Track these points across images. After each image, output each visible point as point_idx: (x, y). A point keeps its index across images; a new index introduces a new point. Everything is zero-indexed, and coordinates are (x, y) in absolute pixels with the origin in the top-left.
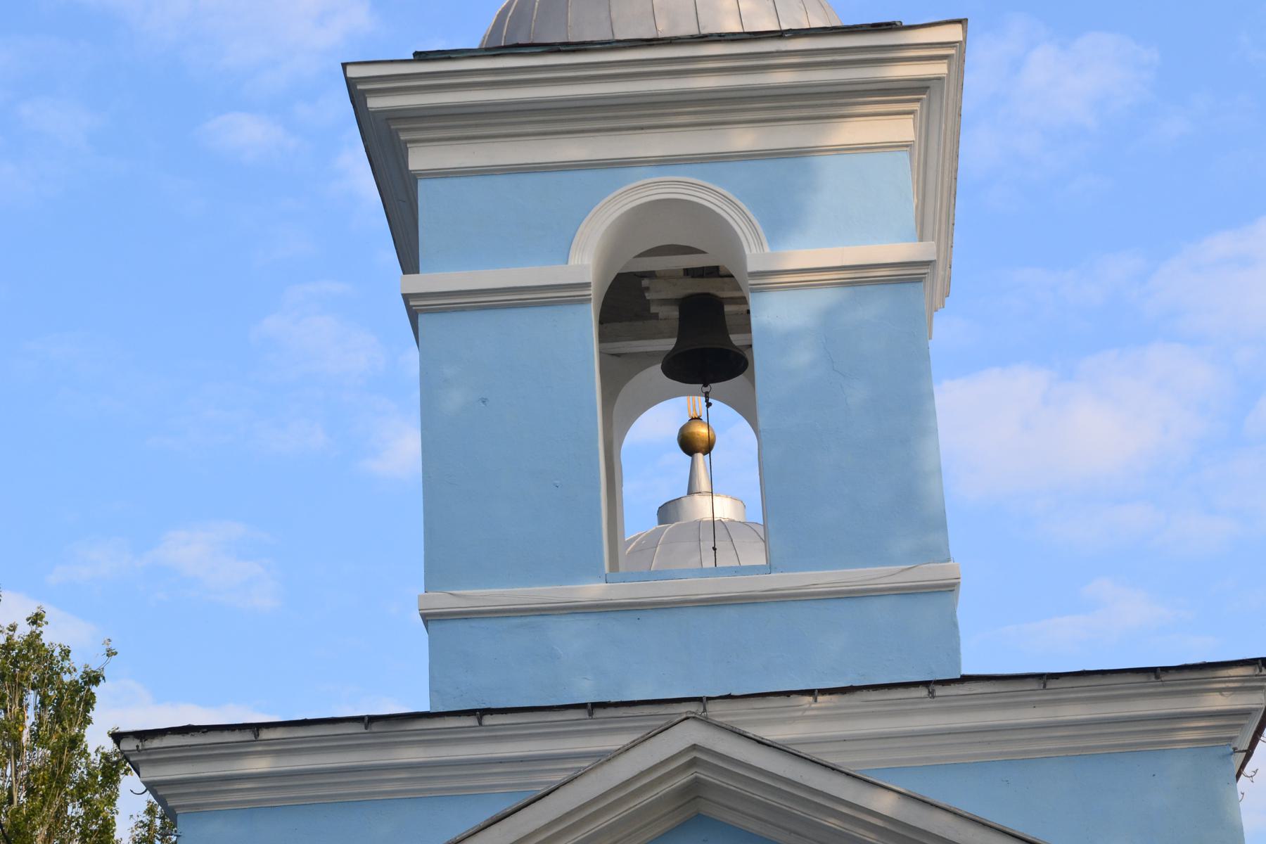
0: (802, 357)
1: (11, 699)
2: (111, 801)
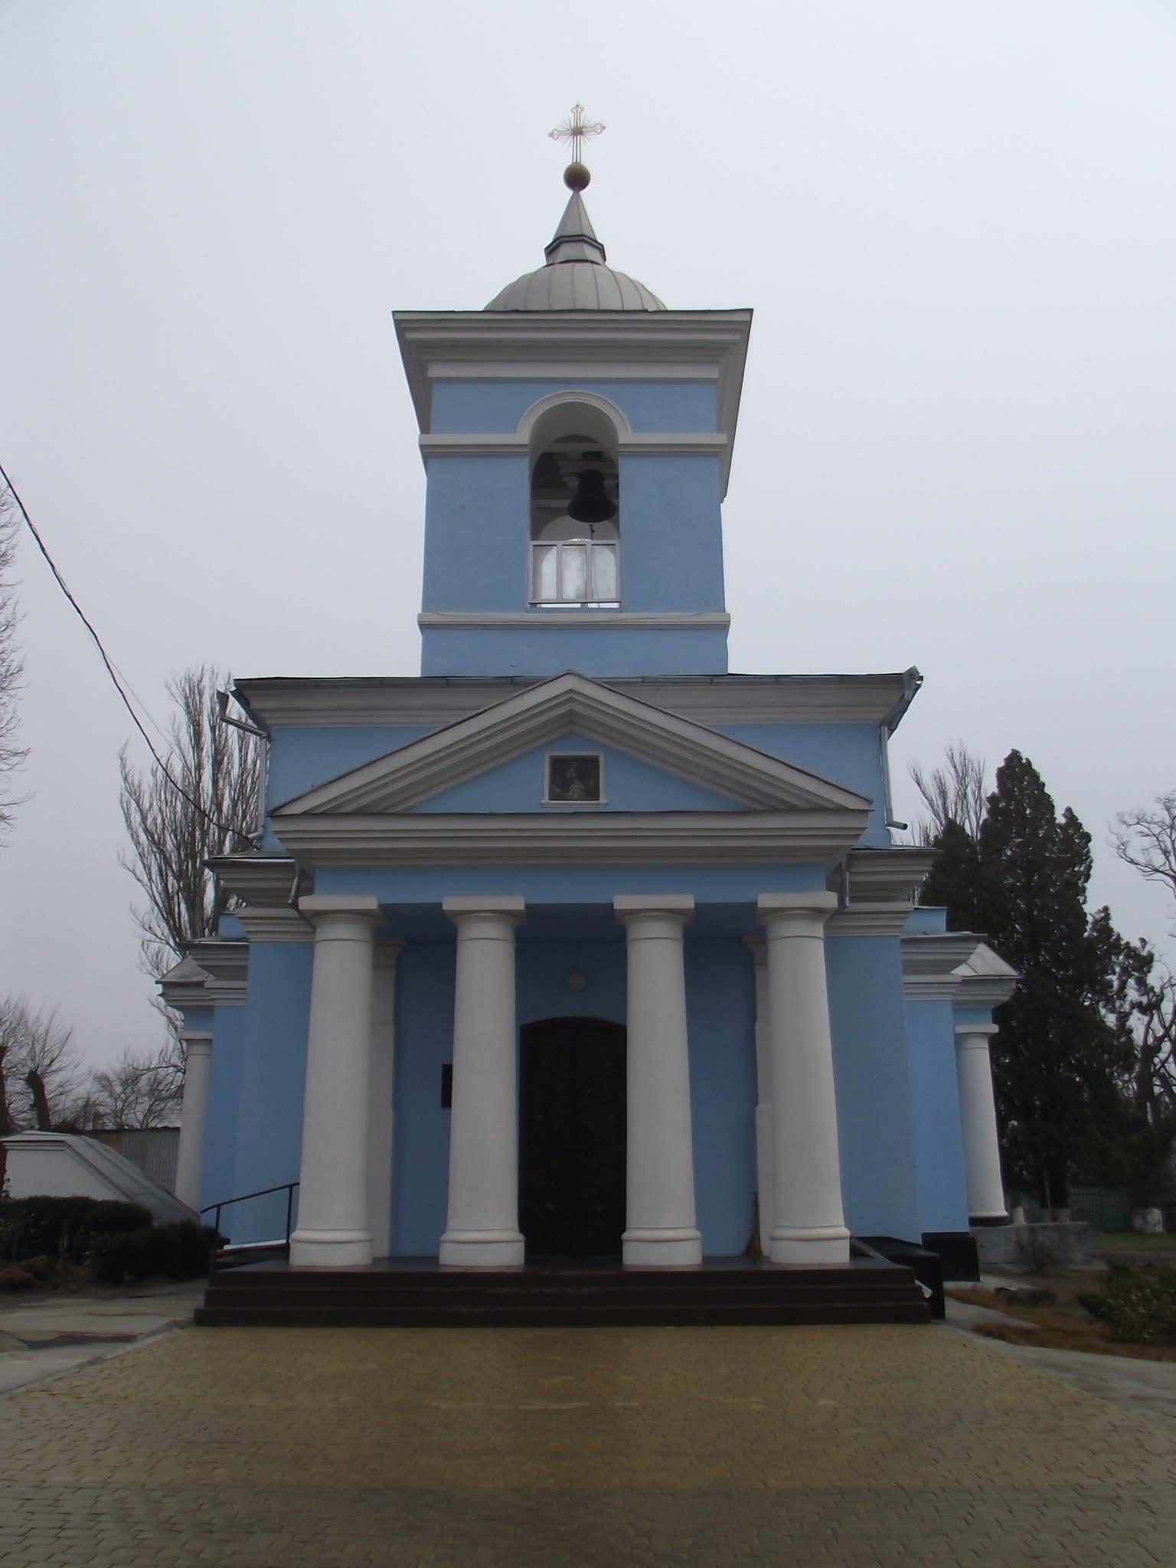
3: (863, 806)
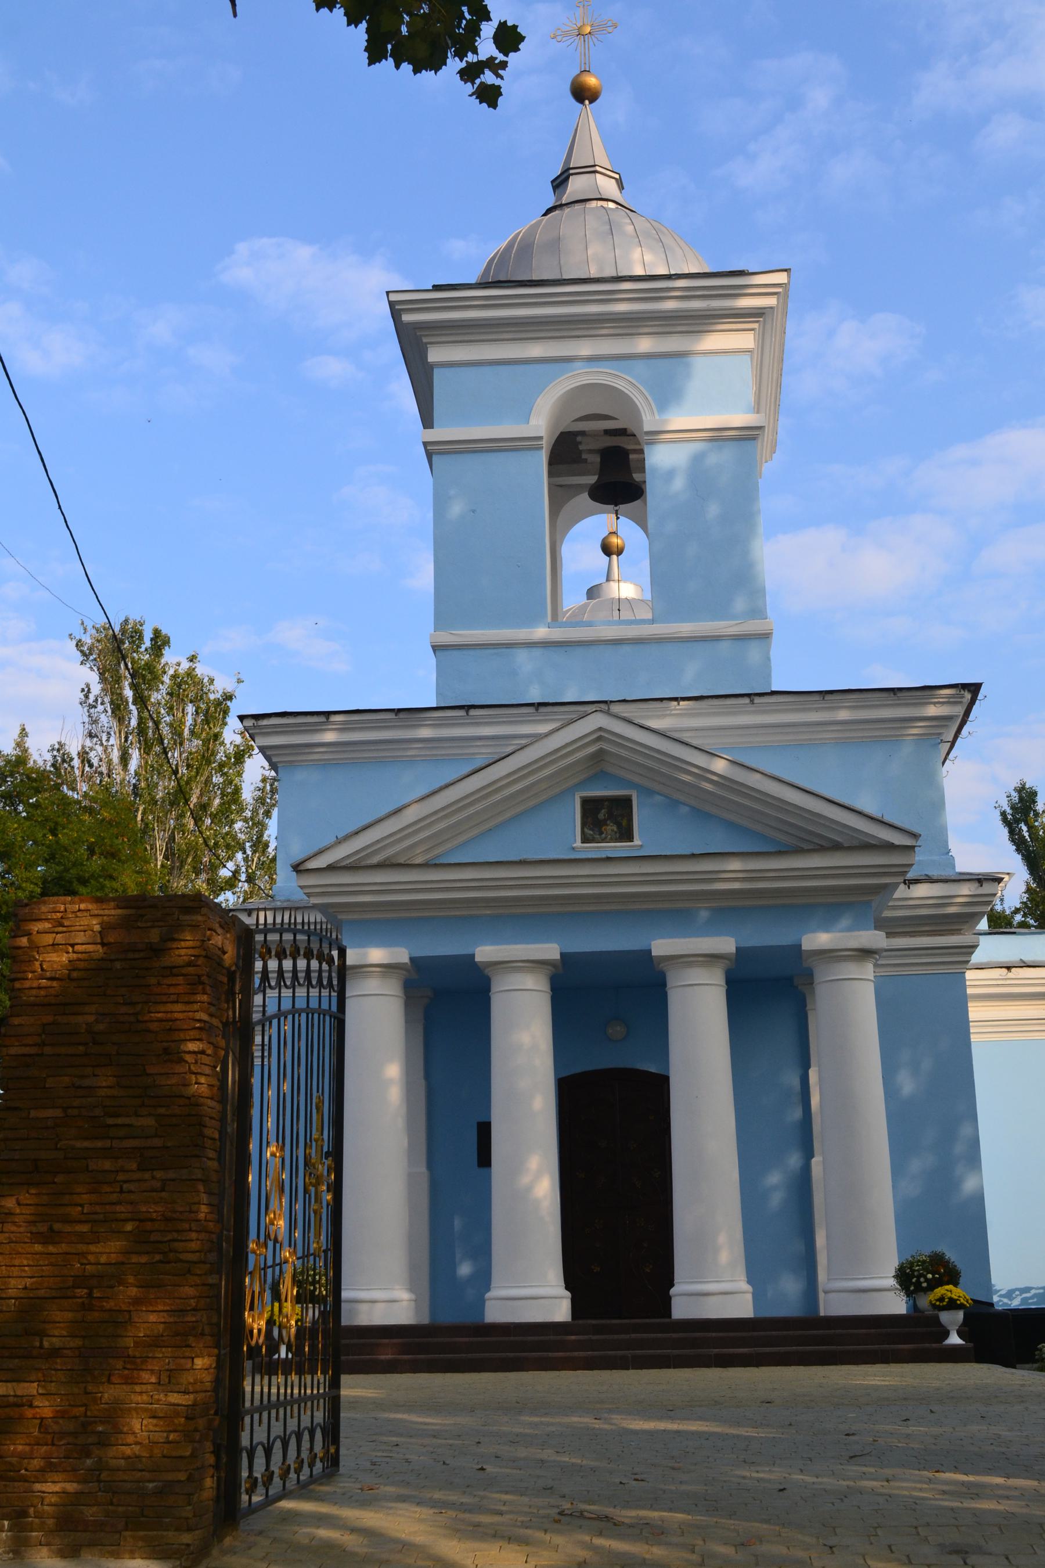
0: (679, 484)
1: (177, 709)
2: (240, 774)
3: (907, 841)
